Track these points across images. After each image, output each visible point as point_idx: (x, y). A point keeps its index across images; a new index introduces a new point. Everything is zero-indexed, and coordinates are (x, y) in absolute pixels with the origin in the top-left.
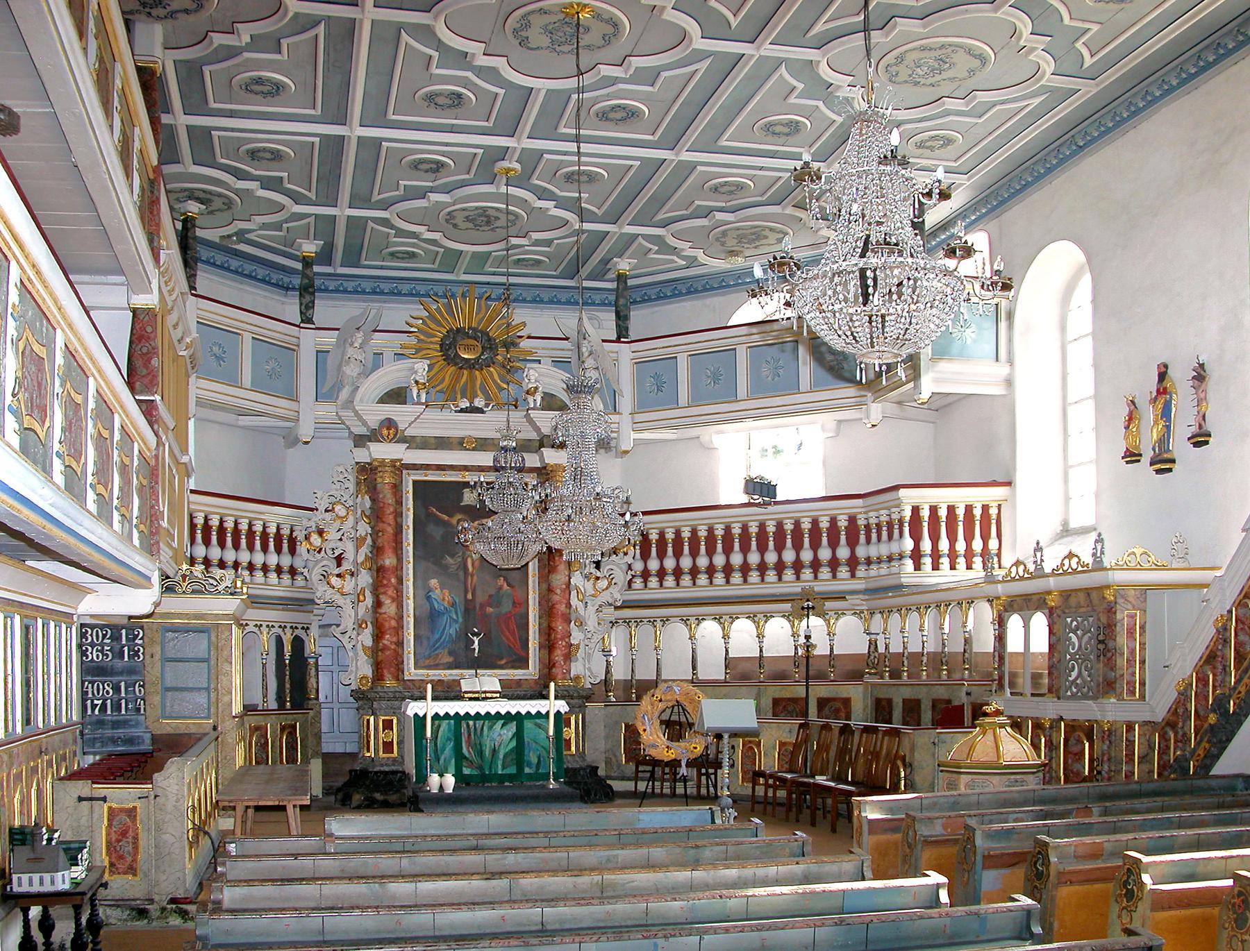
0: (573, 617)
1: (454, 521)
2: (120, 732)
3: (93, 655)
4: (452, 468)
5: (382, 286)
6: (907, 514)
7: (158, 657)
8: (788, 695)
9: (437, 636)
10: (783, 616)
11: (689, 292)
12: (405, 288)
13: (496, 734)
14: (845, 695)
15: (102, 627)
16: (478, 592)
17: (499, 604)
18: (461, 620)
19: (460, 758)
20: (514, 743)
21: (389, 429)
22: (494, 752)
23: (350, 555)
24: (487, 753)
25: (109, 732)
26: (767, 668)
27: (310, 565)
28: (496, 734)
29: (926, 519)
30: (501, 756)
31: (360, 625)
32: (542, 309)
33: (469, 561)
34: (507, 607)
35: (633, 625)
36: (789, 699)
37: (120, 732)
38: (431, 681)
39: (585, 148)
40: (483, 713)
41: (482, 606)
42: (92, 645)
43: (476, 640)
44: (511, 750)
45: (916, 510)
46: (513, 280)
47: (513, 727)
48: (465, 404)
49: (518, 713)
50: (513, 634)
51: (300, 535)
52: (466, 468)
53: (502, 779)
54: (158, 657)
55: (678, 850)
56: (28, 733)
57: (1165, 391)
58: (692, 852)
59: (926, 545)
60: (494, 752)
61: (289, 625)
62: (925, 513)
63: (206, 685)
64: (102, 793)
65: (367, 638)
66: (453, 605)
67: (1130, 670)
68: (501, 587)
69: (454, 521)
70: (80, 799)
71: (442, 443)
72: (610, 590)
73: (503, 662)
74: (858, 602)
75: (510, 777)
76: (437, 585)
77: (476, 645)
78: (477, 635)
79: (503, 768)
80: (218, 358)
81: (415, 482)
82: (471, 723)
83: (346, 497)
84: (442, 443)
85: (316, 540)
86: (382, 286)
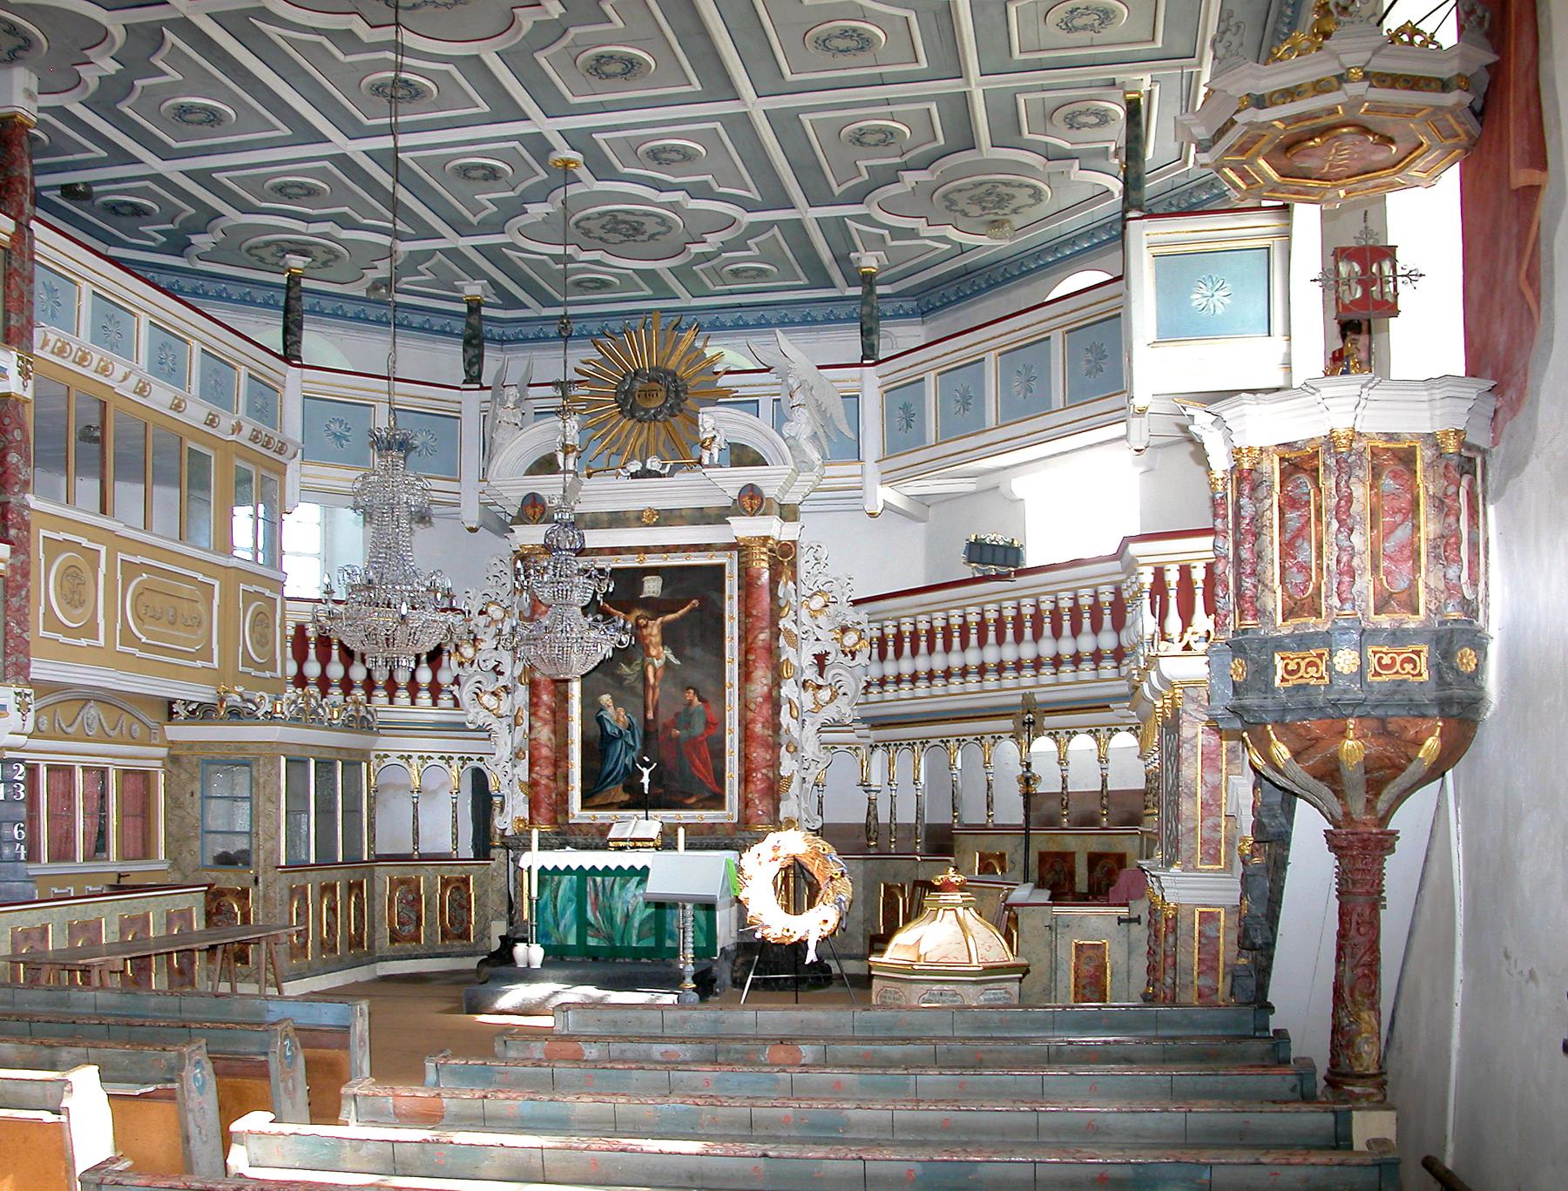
0: (784, 739)
5: (611, 324)
6: (1147, 578)
7: (198, 795)
8: (1055, 849)
9: (609, 767)
10: (1130, 730)
11: (990, 287)
12: (705, 319)
13: (630, 895)
14: (1118, 850)
16: (661, 709)
17: (688, 725)
18: (639, 746)
19: (583, 925)
21: (534, 506)
22: (628, 917)
23: (506, 668)
24: (619, 918)
26: (1075, 809)
27: (462, 680)
28: (630, 895)
29: (1174, 585)
30: (636, 925)
31: (517, 755)
32: (818, 331)
33: (650, 669)
34: (698, 728)
35: (892, 749)
36: (1058, 854)
38: (685, 826)
39: (405, 140)
40: (613, 868)
41: (666, 727)
43: (646, 772)
44: (649, 916)
45: (1159, 573)
46: (572, 311)
48: (635, 466)
50: (705, 765)
52: (647, 550)
53: (637, 954)
54: (198, 795)
55: (29, 1048)
57: (93, 436)
58: (46, 1052)
60: (628, 917)
61: (456, 756)
62: (1172, 577)
63: (247, 829)
66: (630, 727)
67: (1209, 822)
68: (690, 703)
71: (617, 520)
73: (693, 800)
74: (1125, 712)
75: (648, 952)
76: (610, 703)
77: (646, 780)
78: (647, 765)
79: (639, 940)
80: (338, 437)
81: (721, 567)
82: (599, 879)
83: (503, 595)
84: (617, 520)
86: (611, 324)
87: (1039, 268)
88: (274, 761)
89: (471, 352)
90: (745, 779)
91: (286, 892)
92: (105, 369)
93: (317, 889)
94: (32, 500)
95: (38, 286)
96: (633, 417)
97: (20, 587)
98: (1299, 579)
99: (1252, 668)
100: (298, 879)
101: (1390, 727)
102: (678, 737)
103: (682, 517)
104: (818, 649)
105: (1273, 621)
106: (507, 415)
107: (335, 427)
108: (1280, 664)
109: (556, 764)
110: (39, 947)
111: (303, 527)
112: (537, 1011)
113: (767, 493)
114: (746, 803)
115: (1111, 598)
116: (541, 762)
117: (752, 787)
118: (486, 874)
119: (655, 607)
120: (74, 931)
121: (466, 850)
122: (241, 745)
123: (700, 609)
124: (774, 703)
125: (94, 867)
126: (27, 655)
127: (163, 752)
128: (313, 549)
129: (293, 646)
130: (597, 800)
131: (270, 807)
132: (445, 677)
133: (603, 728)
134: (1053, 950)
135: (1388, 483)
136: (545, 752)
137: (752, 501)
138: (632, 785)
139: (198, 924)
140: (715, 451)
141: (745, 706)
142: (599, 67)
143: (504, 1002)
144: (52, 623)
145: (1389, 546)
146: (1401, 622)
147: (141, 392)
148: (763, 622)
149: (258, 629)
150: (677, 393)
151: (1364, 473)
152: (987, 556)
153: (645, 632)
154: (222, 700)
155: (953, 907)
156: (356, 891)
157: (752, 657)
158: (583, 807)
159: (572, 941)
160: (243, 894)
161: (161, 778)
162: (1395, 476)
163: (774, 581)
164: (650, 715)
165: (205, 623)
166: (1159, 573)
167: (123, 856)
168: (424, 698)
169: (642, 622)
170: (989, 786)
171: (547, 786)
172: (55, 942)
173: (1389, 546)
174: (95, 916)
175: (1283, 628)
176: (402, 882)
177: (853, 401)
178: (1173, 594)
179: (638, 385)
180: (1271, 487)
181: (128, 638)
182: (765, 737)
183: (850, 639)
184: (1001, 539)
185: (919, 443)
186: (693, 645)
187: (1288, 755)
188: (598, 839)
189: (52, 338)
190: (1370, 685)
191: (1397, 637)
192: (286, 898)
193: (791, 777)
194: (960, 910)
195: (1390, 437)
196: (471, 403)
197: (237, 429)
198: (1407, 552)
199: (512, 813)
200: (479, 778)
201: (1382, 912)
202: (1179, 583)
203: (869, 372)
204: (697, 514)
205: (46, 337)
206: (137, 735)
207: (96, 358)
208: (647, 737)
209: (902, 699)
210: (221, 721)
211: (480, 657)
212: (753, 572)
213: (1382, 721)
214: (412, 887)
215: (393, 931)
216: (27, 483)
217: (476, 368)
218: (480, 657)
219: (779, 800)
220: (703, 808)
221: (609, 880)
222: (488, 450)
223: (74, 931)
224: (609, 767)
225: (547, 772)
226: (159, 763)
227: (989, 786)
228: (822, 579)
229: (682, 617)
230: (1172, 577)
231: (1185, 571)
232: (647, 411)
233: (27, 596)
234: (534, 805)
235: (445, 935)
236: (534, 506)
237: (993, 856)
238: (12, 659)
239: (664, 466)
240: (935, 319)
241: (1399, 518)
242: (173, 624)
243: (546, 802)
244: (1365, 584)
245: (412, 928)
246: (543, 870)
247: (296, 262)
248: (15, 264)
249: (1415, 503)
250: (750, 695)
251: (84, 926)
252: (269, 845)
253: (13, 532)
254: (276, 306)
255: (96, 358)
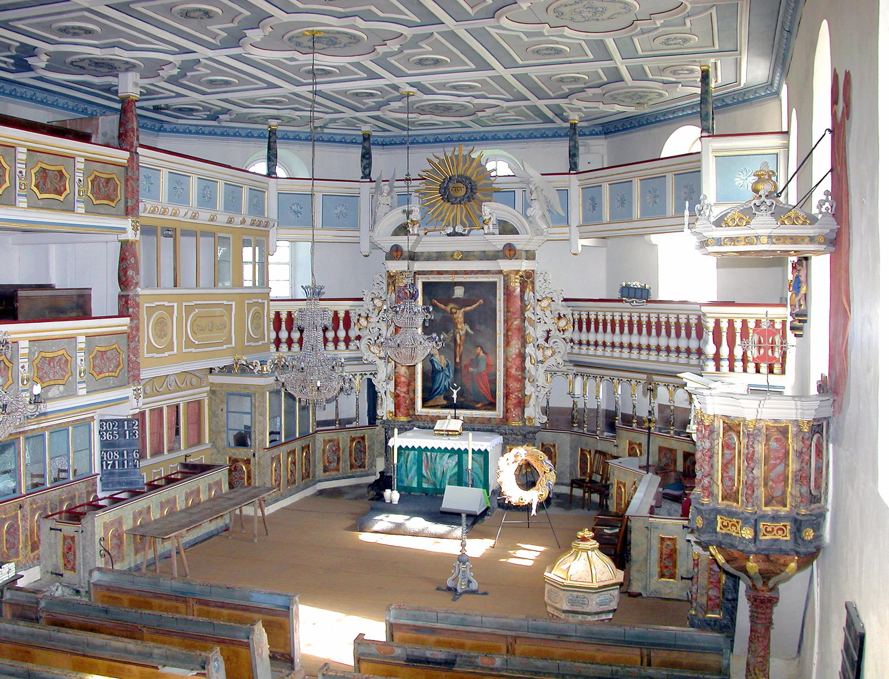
0: (527, 375)
1: (448, 309)
2: (124, 479)
3: (107, 436)
4: (447, 272)
7: (225, 410)
8: (666, 446)
11: (640, 126)
15: (112, 421)
16: (464, 357)
17: (477, 365)
18: (452, 376)
19: (420, 475)
20: (456, 470)
21: (397, 251)
24: (439, 474)
25: (117, 479)
33: (458, 336)
34: (483, 367)
36: (668, 449)
37: (124, 479)
42: (106, 431)
43: (455, 392)
44: (455, 474)
45: (717, 322)
47: (456, 458)
48: (450, 230)
49: (459, 449)
51: (354, 319)
52: (456, 273)
56: (77, 478)
59: (725, 351)
61: (358, 374)
62: (724, 325)
64: (59, 527)
65: (391, 386)
66: (447, 366)
68: (479, 354)
69: (448, 309)
70: (51, 529)
71: (440, 256)
72: (555, 357)
73: (479, 405)
77: (455, 396)
82: (429, 454)
84: (440, 256)
85: (363, 322)
87: (665, 120)
88: (264, 394)
89: (365, 162)
90: (507, 396)
91: (269, 460)
92: (175, 213)
93: (286, 454)
94: (140, 291)
95: (141, 178)
96: (449, 201)
97: (135, 337)
98: (729, 483)
99: (706, 522)
100: (275, 451)
101: (771, 558)
102: (472, 373)
103: (474, 256)
104: (546, 328)
105: (717, 500)
106: (384, 200)
107: (295, 208)
108: (719, 520)
109: (409, 385)
110: (146, 517)
111: (281, 253)
112: (394, 532)
113: (518, 247)
114: (507, 410)
115: (696, 321)
116: (401, 384)
117: (510, 402)
118: (373, 434)
119: (461, 303)
120: (162, 505)
121: (364, 420)
122: (246, 386)
123: (484, 305)
124: (522, 356)
125: (174, 455)
126: (139, 370)
127: (208, 388)
128: (285, 270)
129: (274, 323)
130: (430, 403)
131: (261, 418)
132: (353, 334)
133: (433, 366)
134: (649, 540)
135: (773, 444)
136: (403, 379)
137: (510, 252)
138: (448, 398)
139: (225, 487)
140: (491, 226)
141: (506, 359)
142: (421, 63)
143: (376, 527)
144: (151, 349)
145: (773, 475)
146: (777, 511)
147: (194, 217)
148: (518, 312)
149: (255, 321)
150: (472, 191)
151: (762, 439)
152: (632, 293)
153: (455, 316)
154: (237, 364)
155: (586, 550)
156: (306, 450)
157: (510, 333)
158: (423, 407)
159: (415, 485)
160: (248, 462)
161: (206, 402)
162: (777, 440)
163: (523, 292)
164: (458, 360)
165: (228, 326)
166: (717, 322)
167: (189, 445)
168: (342, 345)
169: (454, 311)
170: (634, 407)
171: (404, 397)
172: (155, 515)
173: (773, 475)
174: (173, 495)
175: (721, 504)
176: (330, 441)
177: (564, 193)
178: (724, 335)
179: (451, 185)
180: (719, 434)
181: (189, 344)
182: (518, 374)
183: (562, 323)
184: (637, 284)
185: (598, 220)
186: (480, 323)
187: (723, 561)
188: (428, 425)
189: (148, 206)
190: (761, 541)
191: (775, 518)
192: (269, 463)
193: (530, 396)
194: (589, 552)
195: (776, 421)
196: (366, 188)
197: (243, 222)
198: (781, 478)
199: (386, 407)
200: (371, 386)
201: (772, 631)
202: (728, 329)
203: (574, 178)
204: (482, 254)
205: (146, 206)
206: (194, 384)
207: (170, 209)
208: (456, 371)
209: (589, 354)
210: (236, 375)
211: (370, 326)
212: (511, 289)
213: (767, 556)
214: (336, 443)
215: (325, 467)
216: (137, 283)
217: (368, 170)
218: (370, 326)
219: (524, 407)
220: (485, 409)
221: (434, 454)
222: (374, 223)
223: (162, 505)
224: (437, 386)
225: (405, 389)
226: (206, 394)
227: (634, 407)
228: (547, 291)
229: (474, 309)
230: (724, 325)
231: (731, 323)
232: (456, 198)
233: (138, 341)
234: (397, 406)
235: (352, 466)
236: (397, 251)
237: (636, 443)
238: (131, 373)
239: (464, 230)
240: (612, 137)
241: (778, 461)
242: (211, 331)
243: (403, 404)
244: (761, 492)
245: (335, 464)
246: (400, 448)
247: (274, 123)
248: (130, 174)
249: (787, 454)
250: (509, 354)
251: (168, 502)
252: (261, 437)
253: (131, 310)
254: (264, 137)
255: (170, 209)
